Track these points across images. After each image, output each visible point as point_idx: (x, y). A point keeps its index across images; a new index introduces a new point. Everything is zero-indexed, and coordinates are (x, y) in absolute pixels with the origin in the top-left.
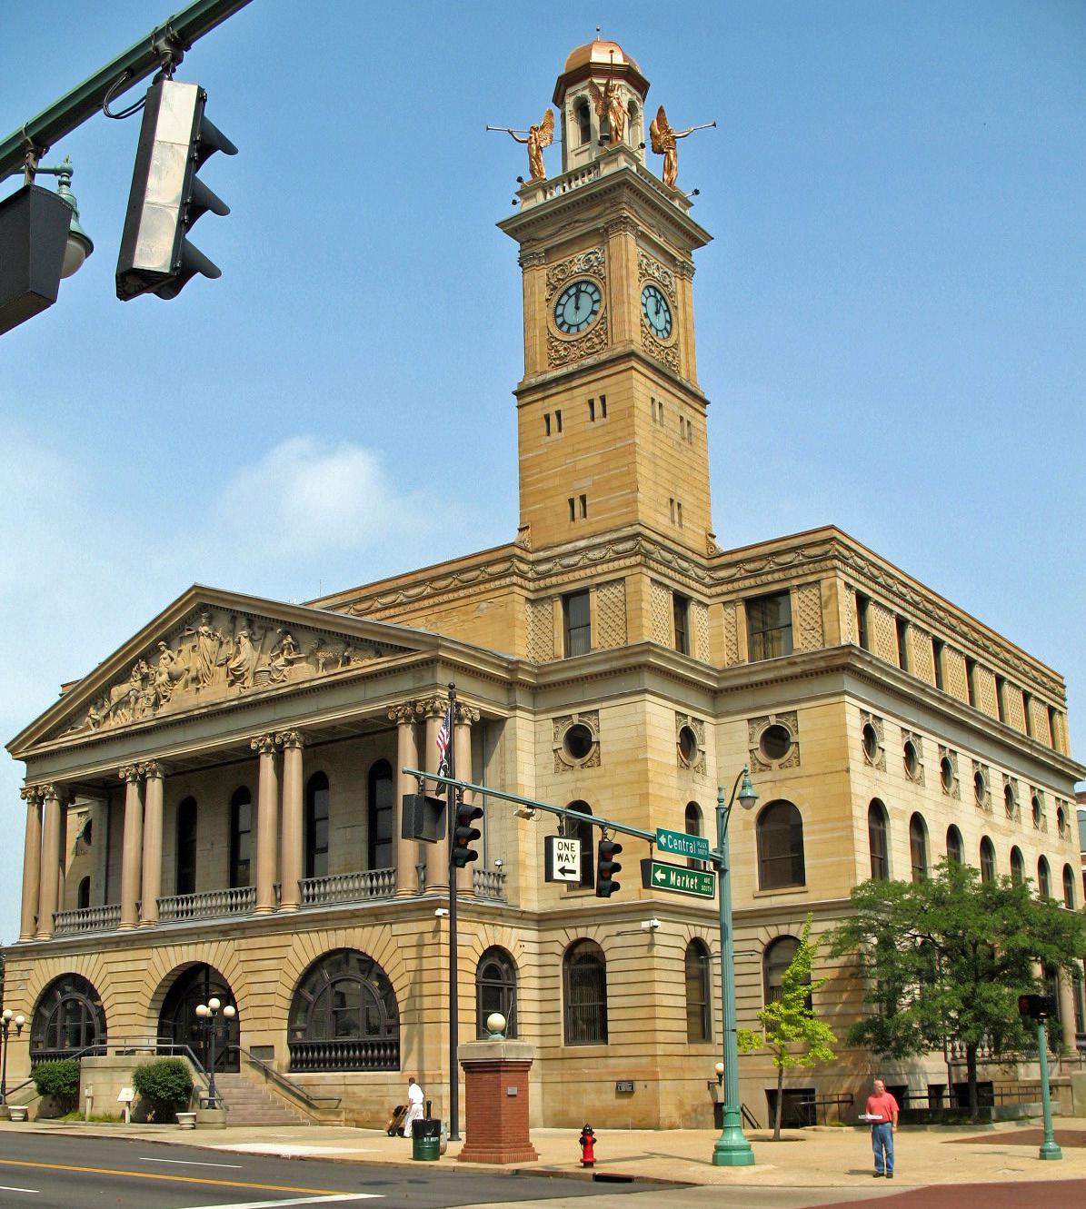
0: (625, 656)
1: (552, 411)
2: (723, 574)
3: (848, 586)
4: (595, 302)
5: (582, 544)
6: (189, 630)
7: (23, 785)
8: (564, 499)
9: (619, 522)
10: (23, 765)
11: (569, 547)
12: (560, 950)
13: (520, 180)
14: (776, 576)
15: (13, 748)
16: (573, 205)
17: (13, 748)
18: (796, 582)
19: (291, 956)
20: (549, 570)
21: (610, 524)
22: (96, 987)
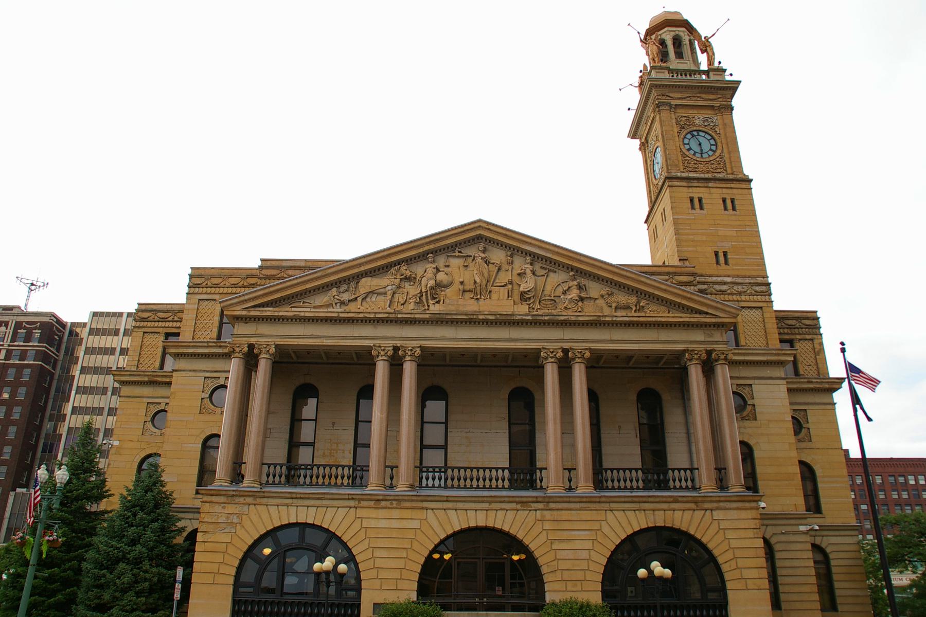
0: (778, 355)
4: (711, 150)
6: (460, 252)
8: (710, 251)
11: (719, 279)
18: (798, 337)
19: (606, 529)
20: (705, 290)
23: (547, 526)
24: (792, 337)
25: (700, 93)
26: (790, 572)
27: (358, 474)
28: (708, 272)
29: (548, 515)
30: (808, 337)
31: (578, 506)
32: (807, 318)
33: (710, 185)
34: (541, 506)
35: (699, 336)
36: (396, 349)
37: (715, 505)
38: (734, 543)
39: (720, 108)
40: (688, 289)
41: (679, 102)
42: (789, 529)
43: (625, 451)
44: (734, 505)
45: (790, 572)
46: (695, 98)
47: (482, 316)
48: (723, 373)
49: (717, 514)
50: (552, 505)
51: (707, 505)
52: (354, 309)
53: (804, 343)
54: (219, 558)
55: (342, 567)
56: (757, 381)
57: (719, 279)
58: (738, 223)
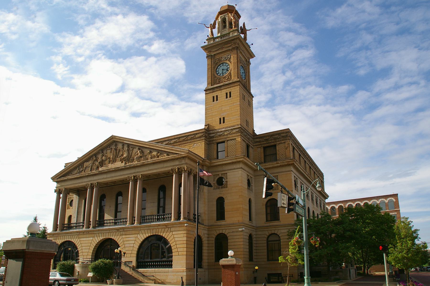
0: (236, 159)
1: (215, 96)
2: (258, 140)
3: (292, 144)
5: (223, 130)
7: (55, 189)
9: (235, 124)
10: (56, 183)
12: (215, 237)
13: (208, 36)
14: (264, 142)
15: (53, 179)
16: (221, 43)
17: (53, 179)
18: (278, 143)
21: (232, 125)
22: (76, 244)
23: (123, 236)
24: (275, 143)
30: (282, 142)
31: (131, 229)
32: (283, 133)
33: (222, 88)
34: (122, 230)
35: (177, 163)
36: (91, 184)
37: (172, 226)
38: (176, 239)
39: (233, 49)
43: (151, 209)
44: (178, 225)
46: (222, 48)
47: (115, 168)
50: (125, 230)
51: (169, 226)
52: (83, 174)
56: (229, 171)
58: (231, 102)
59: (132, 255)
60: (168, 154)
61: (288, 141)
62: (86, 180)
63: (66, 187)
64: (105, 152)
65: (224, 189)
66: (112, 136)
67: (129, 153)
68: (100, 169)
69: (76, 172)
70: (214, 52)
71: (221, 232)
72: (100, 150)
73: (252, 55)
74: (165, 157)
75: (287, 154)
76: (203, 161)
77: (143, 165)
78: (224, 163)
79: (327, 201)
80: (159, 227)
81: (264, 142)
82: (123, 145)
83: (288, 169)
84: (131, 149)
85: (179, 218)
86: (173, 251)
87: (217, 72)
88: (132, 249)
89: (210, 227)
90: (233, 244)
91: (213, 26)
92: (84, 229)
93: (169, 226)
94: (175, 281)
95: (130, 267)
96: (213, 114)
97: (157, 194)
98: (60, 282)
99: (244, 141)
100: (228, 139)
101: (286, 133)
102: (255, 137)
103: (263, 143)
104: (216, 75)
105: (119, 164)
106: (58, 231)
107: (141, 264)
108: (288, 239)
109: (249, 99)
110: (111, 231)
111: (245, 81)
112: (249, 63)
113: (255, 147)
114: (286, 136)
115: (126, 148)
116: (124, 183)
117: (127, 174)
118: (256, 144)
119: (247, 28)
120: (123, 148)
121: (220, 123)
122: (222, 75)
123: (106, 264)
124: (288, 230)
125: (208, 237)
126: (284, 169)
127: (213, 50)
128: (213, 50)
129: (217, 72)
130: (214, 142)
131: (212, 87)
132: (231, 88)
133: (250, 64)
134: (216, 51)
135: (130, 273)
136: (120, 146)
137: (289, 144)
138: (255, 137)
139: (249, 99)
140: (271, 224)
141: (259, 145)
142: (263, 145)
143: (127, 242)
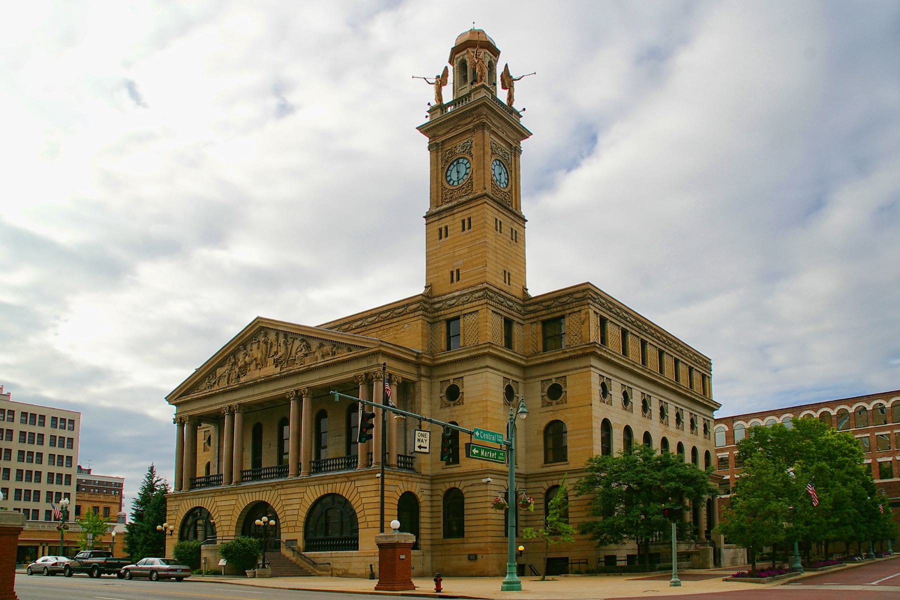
0: (478, 350)
2: (531, 308)
5: (457, 294)
8: (447, 273)
9: (476, 282)
11: (451, 295)
14: (558, 309)
18: (568, 312)
25: (460, 120)
26: (473, 512)
27: (282, 470)
28: (444, 291)
29: (282, 491)
30: (576, 310)
33: (455, 211)
36: (230, 407)
38: (364, 501)
39: (476, 127)
40: (348, 333)
41: (444, 138)
42: (475, 482)
43: (334, 448)
44: (367, 477)
45: (473, 512)
46: (456, 127)
48: (378, 387)
49: (358, 483)
51: (353, 478)
53: (573, 316)
54: (229, 518)
55: (272, 522)
56: (467, 374)
57: (451, 295)
59: (297, 529)
60: (350, 348)
61: (587, 307)
62: (220, 399)
63: (191, 413)
64: (249, 347)
65: (457, 407)
66: (258, 318)
67: (287, 348)
68: (242, 380)
69: (204, 385)
70: (441, 136)
71: (452, 485)
72: (239, 345)
73: (524, 134)
74: (343, 355)
75: (583, 334)
76: (417, 358)
77: (309, 370)
78: (449, 359)
79: (717, 415)
80: (337, 480)
81: (558, 309)
82: (277, 335)
83: (583, 362)
84: (290, 341)
85: (369, 465)
86: (359, 520)
87: (449, 179)
88: (295, 518)
89: (434, 479)
90: (472, 506)
91: (441, 81)
92: (223, 486)
93: (353, 478)
94: (363, 571)
95: (293, 550)
96: (441, 264)
97: (276, 433)
98: (159, 573)
99: (497, 313)
100: (464, 312)
101: (584, 291)
102: (527, 302)
103: (540, 313)
104: (447, 186)
105: (271, 370)
106: (184, 491)
107: (310, 545)
108: (577, 496)
109: (515, 227)
110: (263, 489)
111: (506, 190)
112: (517, 151)
113: (527, 322)
114: (584, 298)
115: (282, 340)
116: (281, 403)
117: (354, 371)
118: (528, 316)
119: (513, 74)
120: (277, 340)
121: (452, 281)
122: (456, 183)
123: (244, 545)
124: (577, 479)
125: (431, 496)
126: (577, 364)
127: (440, 133)
128: (440, 133)
129: (449, 179)
130: (441, 318)
131: (438, 209)
132: (472, 210)
133: (520, 152)
134: (445, 134)
135: (294, 559)
136: (272, 336)
137: (588, 313)
138: (527, 302)
139: (515, 227)
140: (552, 469)
141: (533, 318)
142: (541, 318)
143: (289, 508)
